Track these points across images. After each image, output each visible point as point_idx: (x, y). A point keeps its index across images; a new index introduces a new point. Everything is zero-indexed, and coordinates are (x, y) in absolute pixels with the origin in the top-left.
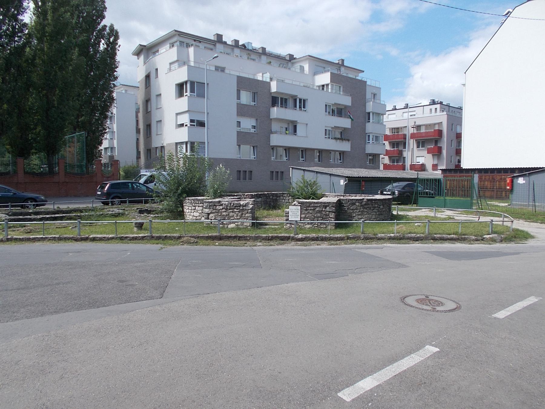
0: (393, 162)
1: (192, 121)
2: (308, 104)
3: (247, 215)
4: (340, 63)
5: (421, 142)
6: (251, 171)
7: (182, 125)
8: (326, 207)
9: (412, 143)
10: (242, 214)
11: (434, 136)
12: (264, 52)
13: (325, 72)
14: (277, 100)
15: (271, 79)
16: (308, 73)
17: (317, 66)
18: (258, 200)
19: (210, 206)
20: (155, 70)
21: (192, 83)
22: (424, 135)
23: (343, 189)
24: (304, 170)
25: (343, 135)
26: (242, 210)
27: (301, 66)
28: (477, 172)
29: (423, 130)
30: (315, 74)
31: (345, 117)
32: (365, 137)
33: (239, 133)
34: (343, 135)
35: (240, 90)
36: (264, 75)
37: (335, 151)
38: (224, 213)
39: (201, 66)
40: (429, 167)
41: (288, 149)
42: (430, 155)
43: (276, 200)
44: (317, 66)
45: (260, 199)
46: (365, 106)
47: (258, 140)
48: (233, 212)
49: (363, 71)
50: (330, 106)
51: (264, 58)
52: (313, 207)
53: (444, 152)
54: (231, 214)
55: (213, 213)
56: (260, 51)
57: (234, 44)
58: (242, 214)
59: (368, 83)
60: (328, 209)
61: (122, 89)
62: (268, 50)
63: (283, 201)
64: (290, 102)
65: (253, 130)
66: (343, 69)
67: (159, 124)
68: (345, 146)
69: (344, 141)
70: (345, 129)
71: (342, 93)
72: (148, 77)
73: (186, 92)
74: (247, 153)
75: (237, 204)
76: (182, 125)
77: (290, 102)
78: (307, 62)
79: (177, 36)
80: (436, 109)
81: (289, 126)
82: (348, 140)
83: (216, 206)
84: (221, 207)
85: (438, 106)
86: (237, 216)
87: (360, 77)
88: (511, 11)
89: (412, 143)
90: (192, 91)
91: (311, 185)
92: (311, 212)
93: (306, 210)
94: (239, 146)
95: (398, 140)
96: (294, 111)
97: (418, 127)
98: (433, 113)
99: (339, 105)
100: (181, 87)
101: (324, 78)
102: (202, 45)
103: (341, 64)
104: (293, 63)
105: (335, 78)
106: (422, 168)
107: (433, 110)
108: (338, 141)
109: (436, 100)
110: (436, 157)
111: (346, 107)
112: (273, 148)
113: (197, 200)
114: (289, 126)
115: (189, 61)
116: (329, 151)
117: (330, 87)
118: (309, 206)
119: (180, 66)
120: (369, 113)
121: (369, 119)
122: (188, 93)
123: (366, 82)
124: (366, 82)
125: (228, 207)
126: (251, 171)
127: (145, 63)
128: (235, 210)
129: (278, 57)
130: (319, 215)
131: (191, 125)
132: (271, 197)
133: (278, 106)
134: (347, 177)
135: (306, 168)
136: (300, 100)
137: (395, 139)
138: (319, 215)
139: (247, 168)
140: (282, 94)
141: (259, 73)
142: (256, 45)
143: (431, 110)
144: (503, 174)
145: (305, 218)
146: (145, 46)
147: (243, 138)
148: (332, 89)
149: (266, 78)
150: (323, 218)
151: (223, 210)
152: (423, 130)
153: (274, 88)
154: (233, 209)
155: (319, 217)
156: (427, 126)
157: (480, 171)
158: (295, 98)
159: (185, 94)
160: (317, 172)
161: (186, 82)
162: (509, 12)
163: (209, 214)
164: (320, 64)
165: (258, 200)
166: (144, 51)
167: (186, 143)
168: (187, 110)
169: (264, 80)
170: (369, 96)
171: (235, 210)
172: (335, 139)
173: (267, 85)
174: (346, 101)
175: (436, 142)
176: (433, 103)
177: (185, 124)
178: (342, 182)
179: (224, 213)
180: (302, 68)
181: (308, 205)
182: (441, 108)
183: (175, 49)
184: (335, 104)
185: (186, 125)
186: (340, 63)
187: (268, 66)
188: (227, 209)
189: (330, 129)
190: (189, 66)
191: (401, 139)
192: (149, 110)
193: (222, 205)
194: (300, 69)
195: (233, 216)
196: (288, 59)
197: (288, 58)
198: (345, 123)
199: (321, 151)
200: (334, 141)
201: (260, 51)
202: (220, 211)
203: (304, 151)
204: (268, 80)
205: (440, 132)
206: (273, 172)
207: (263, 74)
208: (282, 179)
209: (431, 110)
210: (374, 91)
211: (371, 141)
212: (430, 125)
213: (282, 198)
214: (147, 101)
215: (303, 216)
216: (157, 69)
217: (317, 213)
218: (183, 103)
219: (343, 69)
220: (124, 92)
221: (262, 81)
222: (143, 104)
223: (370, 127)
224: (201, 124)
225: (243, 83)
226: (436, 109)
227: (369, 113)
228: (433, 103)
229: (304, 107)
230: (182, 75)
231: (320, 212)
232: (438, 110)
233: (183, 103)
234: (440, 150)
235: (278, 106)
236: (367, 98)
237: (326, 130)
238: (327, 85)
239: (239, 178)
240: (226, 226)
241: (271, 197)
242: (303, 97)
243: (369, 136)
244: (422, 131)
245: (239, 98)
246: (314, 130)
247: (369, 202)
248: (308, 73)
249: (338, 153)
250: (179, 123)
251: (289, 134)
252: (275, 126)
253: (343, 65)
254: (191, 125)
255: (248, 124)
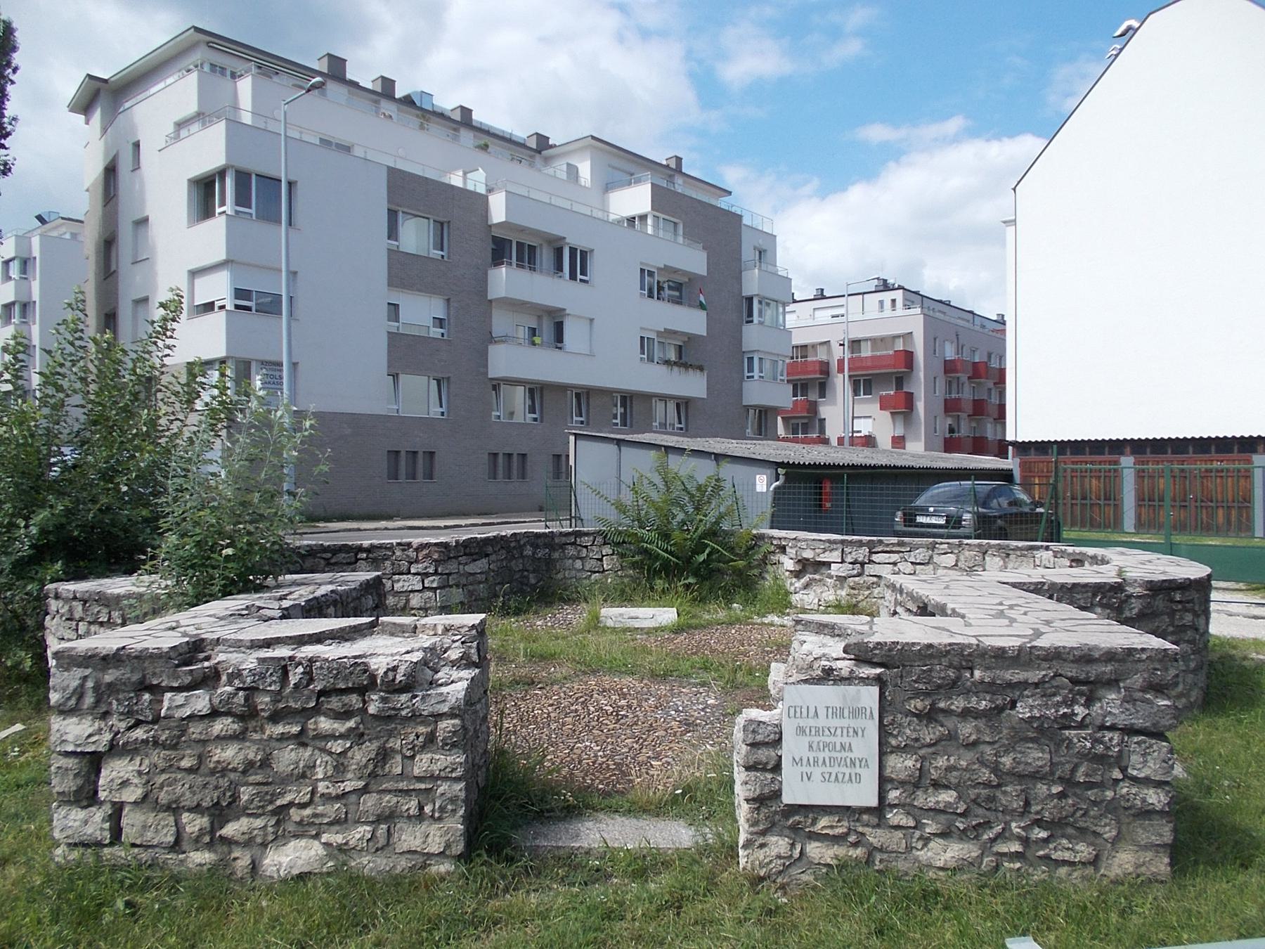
0: (795, 432)
1: (240, 293)
2: (597, 266)
3: (423, 763)
4: (673, 166)
5: (863, 383)
6: (432, 454)
7: (209, 307)
8: (1090, 689)
9: (841, 383)
10: (384, 755)
11: (894, 367)
12: (464, 120)
13: (638, 181)
14: (507, 247)
15: (490, 191)
16: (588, 184)
17: (614, 168)
18: (470, 568)
19: (103, 692)
20: (130, 147)
21: (243, 178)
22: (869, 364)
23: (768, 509)
24: (619, 442)
25: (685, 354)
26: (383, 718)
27: (568, 164)
28: (1032, 450)
29: (866, 351)
30: (608, 187)
31: (690, 306)
32: (741, 361)
33: (393, 337)
34: (685, 354)
35: (396, 212)
36: (469, 175)
37: (664, 398)
38: (229, 754)
39: (272, 127)
40: (884, 441)
41: (538, 392)
42: (887, 414)
43: (549, 562)
44: (614, 168)
45: (479, 566)
46: (739, 279)
47: (453, 357)
48: (301, 739)
49: (730, 193)
50: (651, 274)
51: (466, 136)
52: (990, 688)
53: (920, 406)
54: (287, 758)
55: (129, 750)
56: (457, 116)
57: (379, 90)
58: (384, 755)
59: (746, 221)
60: (1111, 705)
61: (64, 229)
62: (477, 117)
63: (578, 564)
64: (545, 256)
65: (436, 332)
66: (679, 180)
67: (140, 309)
68: (693, 385)
69: (691, 371)
70: (691, 338)
71: (680, 239)
72: (111, 171)
73: (223, 203)
74: (419, 398)
75: (337, 669)
76: (209, 307)
77: (545, 256)
78: (588, 154)
79: (204, 48)
80: (894, 301)
81: (540, 324)
82: (701, 369)
83: (157, 690)
84: (201, 701)
85: (898, 295)
86: (340, 768)
87: (723, 203)
88: (1135, 24)
89: (841, 383)
90: (242, 199)
91: (701, 497)
92: (967, 730)
93: (930, 716)
94: (395, 376)
95: (810, 378)
96: (556, 280)
97: (855, 344)
98: (888, 312)
99: (676, 271)
100: (205, 192)
101: (635, 199)
102: (284, 80)
103: (675, 169)
104: (547, 160)
105: (661, 198)
106: (869, 441)
107: (888, 304)
108: (676, 369)
109: (891, 281)
110: (900, 419)
111: (693, 278)
112: (496, 385)
113: (103, 600)
114: (540, 324)
115: (236, 108)
116: (647, 397)
117: (650, 221)
118: (953, 686)
119: (204, 126)
120: (750, 300)
121: (750, 314)
122: (229, 208)
123: (740, 217)
124: (740, 217)
125: (263, 701)
126: (432, 454)
127: (104, 130)
128: (325, 724)
129: (507, 140)
130: (1036, 757)
131: (237, 307)
132: (528, 551)
133: (511, 264)
134: (781, 465)
135: (628, 437)
136: (573, 251)
137: (798, 373)
138: (1036, 757)
139: (419, 442)
140: (523, 230)
141: (457, 169)
142: (447, 102)
143: (881, 302)
144: (1214, 455)
145: (917, 782)
146: (105, 81)
147: (405, 353)
148: (656, 226)
149: (477, 182)
150: (1069, 782)
151: (221, 726)
152: (866, 351)
153: (498, 211)
154: (306, 714)
155: (1036, 776)
156: (874, 340)
157: (1139, 447)
158: (558, 245)
159: (218, 210)
160: (666, 448)
161: (222, 173)
162: (1129, 28)
163: (94, 762)
164: (622, 163)
165: (470, 568)
166: (102, 94)
167: (223, 361)
168: (223, 257)
169: (470, 187)
170: (748, 253)
171: (325, 724)
172: (667, 362)
173: (479, 203)
174: (694, 261)
175: (900, 381)
176: (885, 286)
177: (217, 304)
178: (762, 483)
179: (229, 754)
180: (573, 171)
181: (941, 672)
182: (905, 299)
183: (194, 76)
184: (667, 269)
185: (222, 307)
186: (673, 166)
187: (481, 155)
188: (248, 715)
189: (653, 336)
190: (234, 125)
191: (815, 372)
192: (113, 268)
193: (210, 679)
194: (568, 173)
195: (303, 775)
196: (534, 146)
197: (533, 144)
198: (692, 321)
199: (627, 398)
200: (664, 368)
201: (457, 116)
202: (195, 730)
203: (584, 396)
204: (481, 190)
205: (908, 357)
206: (496, 455)
207: (465, 174)
208: (523, 475)
209: (881, 302)
210: (761, 243)
211: (756, 374)
212: (882, 339)
213: (571, 551)
214: (108, 244)
215: (902, 765)
216: (137, 145)
217: (1019, 737)
218: (212, 239)
219: (679, 180)
220: (68, 236)
221: (463, 192)
222: (97, 252)
223: (753, 337)
224: (270, 306)
225: (408, 194)
226: (894, 301)
227: (750, 300)
228: (885, 286)
229: (583, 272)
230: (209, 150)
231: (1047, 732)
232: (899, 303)
233: (212, 239)
234: (909, 400)
235: (511, 264)
236: (744, 258)
237: (642, 338)
238: (643, 218)
239: (394, 475)
240: (242, 859)
241: (528, 551)
242: (580, 242)
243: (751, 360)
244: (863, 354)
245: (393, 233)
246: (611, 339)
247: (1160, 603)
248: (588, 184)
249: (672, 406)
250: (199, 301)
251: (541, 345)
252: (501, 323)
253: (678, 169)
254: (237, 307)
255: (421, 312)
